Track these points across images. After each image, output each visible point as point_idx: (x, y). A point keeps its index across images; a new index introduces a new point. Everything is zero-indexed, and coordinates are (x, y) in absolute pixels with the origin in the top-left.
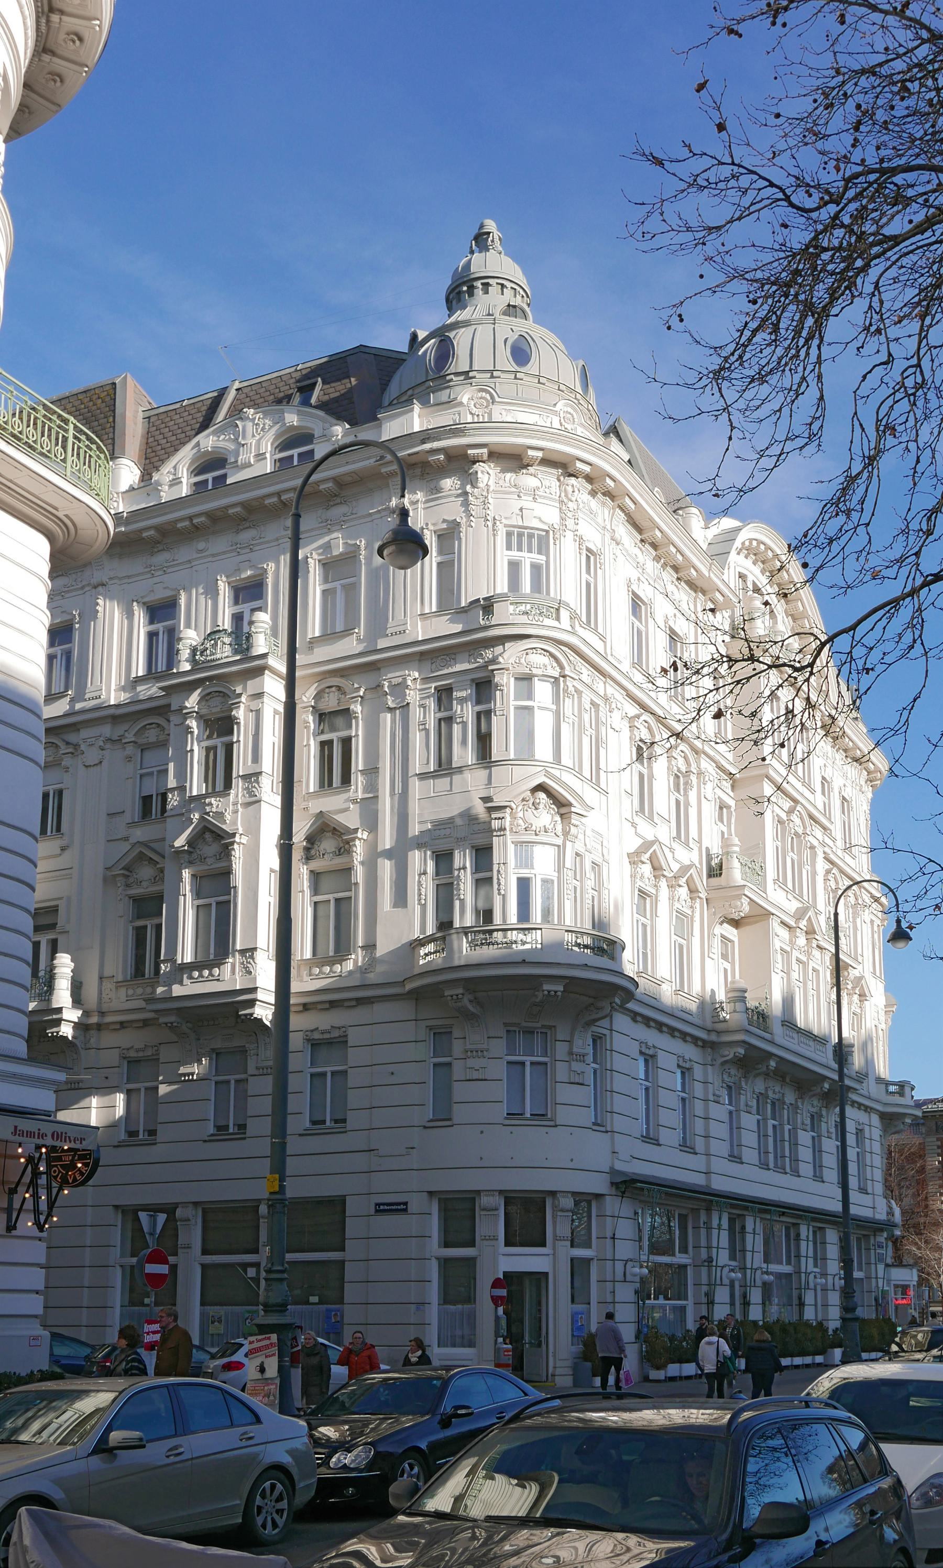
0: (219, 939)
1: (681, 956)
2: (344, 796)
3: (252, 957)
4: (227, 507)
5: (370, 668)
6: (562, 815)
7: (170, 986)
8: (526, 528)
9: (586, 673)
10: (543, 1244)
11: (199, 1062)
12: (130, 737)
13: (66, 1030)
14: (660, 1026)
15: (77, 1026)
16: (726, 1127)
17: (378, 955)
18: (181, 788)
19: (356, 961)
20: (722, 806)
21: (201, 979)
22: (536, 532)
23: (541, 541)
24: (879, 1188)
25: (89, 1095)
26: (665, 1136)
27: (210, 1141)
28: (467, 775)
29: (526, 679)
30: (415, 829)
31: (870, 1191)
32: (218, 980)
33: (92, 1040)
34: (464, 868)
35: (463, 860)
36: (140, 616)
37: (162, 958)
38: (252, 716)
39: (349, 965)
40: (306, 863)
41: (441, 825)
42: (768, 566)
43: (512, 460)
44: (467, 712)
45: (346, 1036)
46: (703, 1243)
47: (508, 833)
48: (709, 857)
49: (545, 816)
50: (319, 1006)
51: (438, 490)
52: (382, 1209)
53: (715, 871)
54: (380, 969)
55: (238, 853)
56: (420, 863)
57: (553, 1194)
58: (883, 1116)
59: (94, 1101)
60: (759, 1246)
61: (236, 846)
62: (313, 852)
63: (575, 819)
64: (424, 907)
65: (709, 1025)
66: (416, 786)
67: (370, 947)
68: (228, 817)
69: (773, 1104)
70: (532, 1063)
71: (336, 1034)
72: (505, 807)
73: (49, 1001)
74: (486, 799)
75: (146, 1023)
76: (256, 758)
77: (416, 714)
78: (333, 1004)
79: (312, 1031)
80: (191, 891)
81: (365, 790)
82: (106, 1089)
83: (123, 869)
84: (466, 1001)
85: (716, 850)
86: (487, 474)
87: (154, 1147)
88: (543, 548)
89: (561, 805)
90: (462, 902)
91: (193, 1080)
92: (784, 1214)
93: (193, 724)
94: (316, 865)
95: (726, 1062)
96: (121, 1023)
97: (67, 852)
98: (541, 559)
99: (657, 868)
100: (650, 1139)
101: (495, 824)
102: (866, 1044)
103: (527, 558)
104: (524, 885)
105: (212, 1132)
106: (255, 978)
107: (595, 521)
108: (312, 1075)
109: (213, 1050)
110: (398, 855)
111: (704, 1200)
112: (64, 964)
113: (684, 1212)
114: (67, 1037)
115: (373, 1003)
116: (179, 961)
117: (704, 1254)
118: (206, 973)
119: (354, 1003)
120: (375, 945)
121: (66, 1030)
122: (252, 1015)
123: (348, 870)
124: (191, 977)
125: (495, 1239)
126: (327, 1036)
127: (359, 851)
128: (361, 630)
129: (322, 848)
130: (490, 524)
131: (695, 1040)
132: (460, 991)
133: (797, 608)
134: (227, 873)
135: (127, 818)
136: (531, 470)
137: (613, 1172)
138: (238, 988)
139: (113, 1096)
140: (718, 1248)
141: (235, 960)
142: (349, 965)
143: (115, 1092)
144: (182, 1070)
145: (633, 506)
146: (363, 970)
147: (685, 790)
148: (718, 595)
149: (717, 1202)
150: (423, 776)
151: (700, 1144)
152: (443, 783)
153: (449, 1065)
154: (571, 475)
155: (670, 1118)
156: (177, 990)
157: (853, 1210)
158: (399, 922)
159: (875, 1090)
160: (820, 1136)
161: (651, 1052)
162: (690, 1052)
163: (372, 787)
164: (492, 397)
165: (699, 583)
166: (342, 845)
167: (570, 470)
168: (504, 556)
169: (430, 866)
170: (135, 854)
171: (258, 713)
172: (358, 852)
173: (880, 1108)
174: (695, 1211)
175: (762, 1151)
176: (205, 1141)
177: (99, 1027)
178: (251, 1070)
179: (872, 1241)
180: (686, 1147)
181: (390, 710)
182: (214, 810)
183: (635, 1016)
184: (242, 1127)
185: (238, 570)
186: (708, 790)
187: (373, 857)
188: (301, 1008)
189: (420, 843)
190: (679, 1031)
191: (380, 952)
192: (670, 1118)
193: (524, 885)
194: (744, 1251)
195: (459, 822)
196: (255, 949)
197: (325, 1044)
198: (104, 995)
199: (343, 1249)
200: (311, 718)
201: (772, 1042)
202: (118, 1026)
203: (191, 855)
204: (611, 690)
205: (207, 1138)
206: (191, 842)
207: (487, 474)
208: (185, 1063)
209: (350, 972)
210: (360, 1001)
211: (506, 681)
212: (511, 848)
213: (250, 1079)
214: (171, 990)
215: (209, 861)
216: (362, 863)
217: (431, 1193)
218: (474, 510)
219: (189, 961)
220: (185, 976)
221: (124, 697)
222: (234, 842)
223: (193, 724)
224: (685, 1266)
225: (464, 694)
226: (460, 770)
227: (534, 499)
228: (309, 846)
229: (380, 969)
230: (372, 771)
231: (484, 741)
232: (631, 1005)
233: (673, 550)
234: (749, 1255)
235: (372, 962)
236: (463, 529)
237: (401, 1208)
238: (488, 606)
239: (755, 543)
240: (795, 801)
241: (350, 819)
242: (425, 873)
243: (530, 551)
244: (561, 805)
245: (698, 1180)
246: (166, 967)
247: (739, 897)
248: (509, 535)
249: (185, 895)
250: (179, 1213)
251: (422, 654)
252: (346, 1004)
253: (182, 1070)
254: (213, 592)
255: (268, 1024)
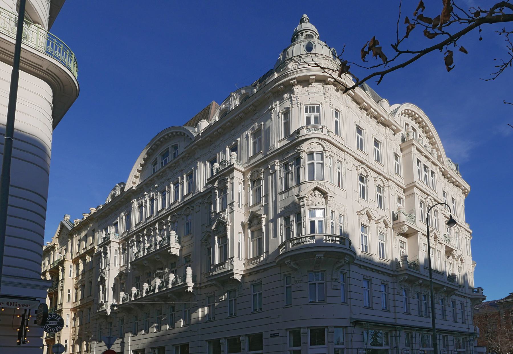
0: (225, 256)
1: (382, 247)
2: (259, 205)
4: (226, 124)
5: (264, 163)
6: (325, 198)
8: (312, 104)
9: (335, 150)
10: (324, 344)
12: (206, 201)
13: (190, 290)
14: (372, 270)
15: (193, 288)
16: (417, 306)
18: (215, 212)
20: (399, 199)
22: (316, 105)
23: (317, 108)
24: (470, 322)
26: (458, 320)
28: (293, 190)
29: (311, 155)
30: (279, 211)
31: (467, 323)
34: (293, 221)
35: (293, 218)
36: (208, 164)
38: (231, 185)
39: (262, 259)
41: (286, 208)
42: (414, 117)
43: (305, 82)
44: (293, 169)
46: (394, 341)
47: (306, 206)
48: (393, 214)
49: (319, 198)
51: (283, 99)
52: (272, 336)
53: (395, 219)
55: (229, 228)
56: (281, 222)
57: (327, 327)
58: (471, 299)
60: (441, 342)
63: (329, 198)
64: (282, 236)
65: (394, 269)
66: (279, 197)
67: (267, 252)
68: (226, 218)
69: (424, 296)
70: (318, 284)
72: (304, 197)
74: (298, 196)
76: (233, 198)
77: (278, 173)
78: (257, 272)
81: (265, 202)
82: (202, 306)
84: (292, 264)
85: (396, 211)
86: (298, 89)
88: (318, 110)
89: (324, 194)
90: (293, 232)
92: (429, 331)
93: (217, 191)
94: (252, 229)
95: (401, 281)
96: (205, 286)
98: (317, 114)
99: (369, 217)
100: (408, 313)
101: (301, 204)
102: (465, 276)
103: (312, 115)
104: (312, 223)
107: (340, 100)
110: (274, 221)
111: (394, 327)
112: (189, 270)
113: (387, 332)
117: (394, 345)
119: (263, 271)
121: (190, 290)
125: (307, 343)
127: (264, 221)
128: (262, 152)
130: (299, 105)
131: (389, 274)
132: (289, 261)
133: (426, 129)
134: (226, 235)
136: (313, 84)
137: (351, 318)
140: (352, 341)
142: (262, 259)
145: (353, 94)
147: (366, 182)
148: (393, 126)
149: (365, 324)
150: (281, 193)
151: (392, 309)
152: (286, 194)
153: (291, 287)
154: (327, 84)
155: (459, 316)
156: (215, 273)
157: (437, 327)
158: (275, 242)
159: (468, 291)
160: (445, 306)
161: (386, 283)
162: (386, 278)
163: (267, 201)
164: (299, 63)
165: (386, 123)
167: (327, 82)
168: (305, 115)
169: (284, 222)
171: (233, 183)
173: (470, 297)
174: (391, 331)
175: (420, 311)
177: (201, 288)
178: (237, 296)
179: (468, 339)
180: (464, 323)
181: (271, 174)
183: (356, 264)
184: (235, 313)
185: (231, 143)
186: (393, 192)
187: (268, 222)
189: (280, 215)
190: (363, 266)
191: (270, 253)
192: (459, 316)
193: (312, 223)
194: (412, 344)
195: (291, 206)
197: (255, 285)
199: (262, 349)
200: (250, 183)
201: (420, 274)
203: (216, 232)
204: (347, 156)
206: (216, 227)
207: (298, 89)
210: (265, 270)
211: (305, 156)
212: (307, 212)
217: (286, 330)
218: (294, 102)
221: (204, 189)
223: (217, 191)
224: (388, 350)
225: (292, 163)
226: (291, 189)
227: (315, 93)
229: (270, 258)
230: (267, 196)
231: (298, 176)
232: (355, 261)
233: (373, 110)
234: (414, 345)
236: (291, 109)
237: (277, 335)
238: (298, 132)
239: (410, 112)
240: (428, 195)
241: (261, 212)
242: (282, 225)
243: (314, 112)
244: (324, 194)
245: (392, 321)
247: (403, 225)
248: (306, 108)
250: (221, 341)
251: (279, 153)
253: (220, 298)
254: (225, 152)
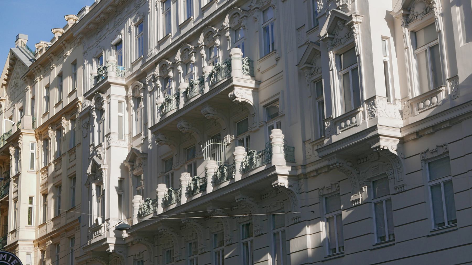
3: (374, 104)
7: (330, 137)
11: (361, 190)
13: (283, 182)
15: (290, 177)
17: (460, 83)
19: (446, 91)
21: (347, 128)
25: (303, 227)
27: (375, 249)
32: (356, 126)
33: (303, 187)
37: (325, 118)
39: (442, 96)
40: (407, 26)
45: (448, 152)
50: (427, 132)
54: (462, 93)
59: (308, 230)
61: (355, 25)
62: (410, 17)
67: (454, 78)
68: (349, 6)
71: (441, 151)
73: (271, 163)
75: (329, 168)
79: (425, 152)
80: (336, 66)
82: (313, 221)
83: (306, 63)
87: (343, 258)
91: (359, 205)
94: (413, 26)
97: (280, 61)
105: (376, 242)
106: (377, 119)
108: (432, 187)
109: (369, 180)
112: (278, 137)
114: (284, 187)
115: (461, 121)
116: (334, 117)
118: (348, 122)
120: (457, 76)
121: (283, 182)
122: (379, 147)
123: (433, 24)
124: (341, 128)
126: (435, 155)
129: (415, 12)
135: (307, 28)
138: (368, 128)
139: (318, 224)
141: (364, 108)
142: (442, 96)
143: (318, 221)
144: (353, 198)
146: (451, 97)
156: (335, 138)
166: (427, 6)
170: (311, 50)
172: (437, 7)
176: (371, 250)
177: (306, 176)
178: (392, 191)
182: (341, 4)
188: (415, 136)
191: (462, 79)
196: (374, 97)
198: (307, 154)
202: (314, 174)
205: (373, 248)
208: (355, 192)
209: (444, 101)
213: (393, 198)
214: (331, 140)
215: (343, 41)
216: (442, 15)
219: (340, 114)
220: (338, 127)
222: (353, 22)
228: (407, 13)
229: (462, 93)
235: (457, 88)
246: (328, 124)
249: (332, 70)
252: (443, 126)
253: (353, 198)
255: (396, 153)
